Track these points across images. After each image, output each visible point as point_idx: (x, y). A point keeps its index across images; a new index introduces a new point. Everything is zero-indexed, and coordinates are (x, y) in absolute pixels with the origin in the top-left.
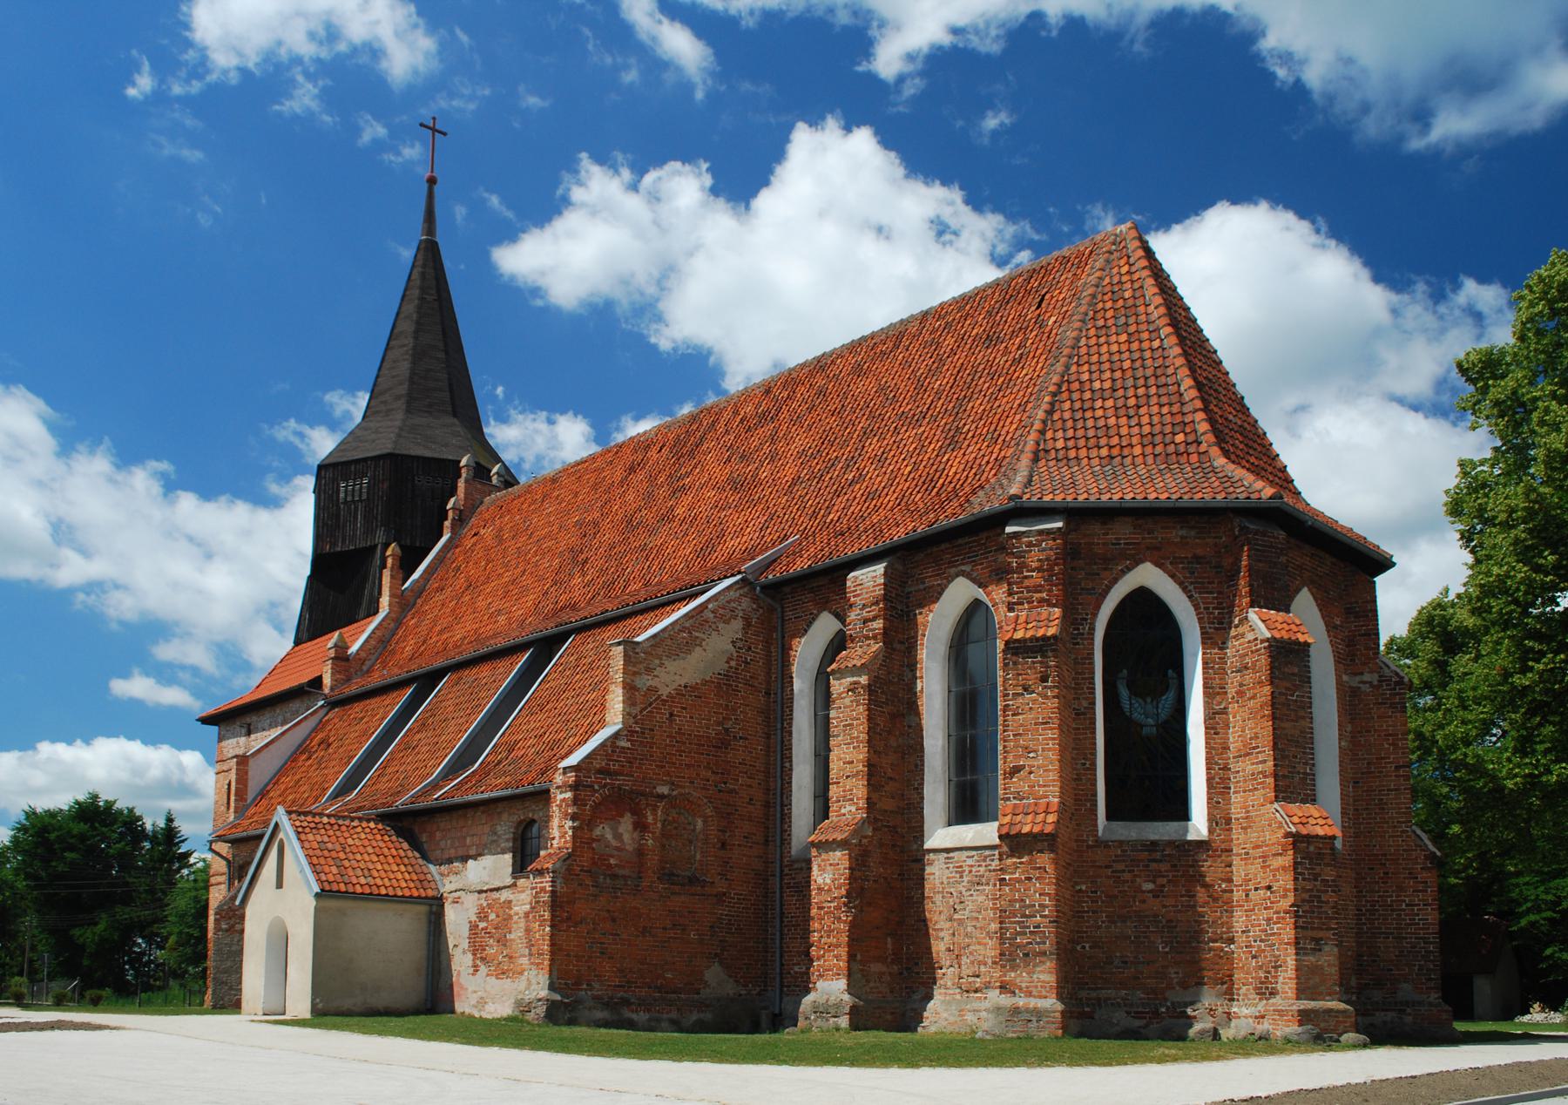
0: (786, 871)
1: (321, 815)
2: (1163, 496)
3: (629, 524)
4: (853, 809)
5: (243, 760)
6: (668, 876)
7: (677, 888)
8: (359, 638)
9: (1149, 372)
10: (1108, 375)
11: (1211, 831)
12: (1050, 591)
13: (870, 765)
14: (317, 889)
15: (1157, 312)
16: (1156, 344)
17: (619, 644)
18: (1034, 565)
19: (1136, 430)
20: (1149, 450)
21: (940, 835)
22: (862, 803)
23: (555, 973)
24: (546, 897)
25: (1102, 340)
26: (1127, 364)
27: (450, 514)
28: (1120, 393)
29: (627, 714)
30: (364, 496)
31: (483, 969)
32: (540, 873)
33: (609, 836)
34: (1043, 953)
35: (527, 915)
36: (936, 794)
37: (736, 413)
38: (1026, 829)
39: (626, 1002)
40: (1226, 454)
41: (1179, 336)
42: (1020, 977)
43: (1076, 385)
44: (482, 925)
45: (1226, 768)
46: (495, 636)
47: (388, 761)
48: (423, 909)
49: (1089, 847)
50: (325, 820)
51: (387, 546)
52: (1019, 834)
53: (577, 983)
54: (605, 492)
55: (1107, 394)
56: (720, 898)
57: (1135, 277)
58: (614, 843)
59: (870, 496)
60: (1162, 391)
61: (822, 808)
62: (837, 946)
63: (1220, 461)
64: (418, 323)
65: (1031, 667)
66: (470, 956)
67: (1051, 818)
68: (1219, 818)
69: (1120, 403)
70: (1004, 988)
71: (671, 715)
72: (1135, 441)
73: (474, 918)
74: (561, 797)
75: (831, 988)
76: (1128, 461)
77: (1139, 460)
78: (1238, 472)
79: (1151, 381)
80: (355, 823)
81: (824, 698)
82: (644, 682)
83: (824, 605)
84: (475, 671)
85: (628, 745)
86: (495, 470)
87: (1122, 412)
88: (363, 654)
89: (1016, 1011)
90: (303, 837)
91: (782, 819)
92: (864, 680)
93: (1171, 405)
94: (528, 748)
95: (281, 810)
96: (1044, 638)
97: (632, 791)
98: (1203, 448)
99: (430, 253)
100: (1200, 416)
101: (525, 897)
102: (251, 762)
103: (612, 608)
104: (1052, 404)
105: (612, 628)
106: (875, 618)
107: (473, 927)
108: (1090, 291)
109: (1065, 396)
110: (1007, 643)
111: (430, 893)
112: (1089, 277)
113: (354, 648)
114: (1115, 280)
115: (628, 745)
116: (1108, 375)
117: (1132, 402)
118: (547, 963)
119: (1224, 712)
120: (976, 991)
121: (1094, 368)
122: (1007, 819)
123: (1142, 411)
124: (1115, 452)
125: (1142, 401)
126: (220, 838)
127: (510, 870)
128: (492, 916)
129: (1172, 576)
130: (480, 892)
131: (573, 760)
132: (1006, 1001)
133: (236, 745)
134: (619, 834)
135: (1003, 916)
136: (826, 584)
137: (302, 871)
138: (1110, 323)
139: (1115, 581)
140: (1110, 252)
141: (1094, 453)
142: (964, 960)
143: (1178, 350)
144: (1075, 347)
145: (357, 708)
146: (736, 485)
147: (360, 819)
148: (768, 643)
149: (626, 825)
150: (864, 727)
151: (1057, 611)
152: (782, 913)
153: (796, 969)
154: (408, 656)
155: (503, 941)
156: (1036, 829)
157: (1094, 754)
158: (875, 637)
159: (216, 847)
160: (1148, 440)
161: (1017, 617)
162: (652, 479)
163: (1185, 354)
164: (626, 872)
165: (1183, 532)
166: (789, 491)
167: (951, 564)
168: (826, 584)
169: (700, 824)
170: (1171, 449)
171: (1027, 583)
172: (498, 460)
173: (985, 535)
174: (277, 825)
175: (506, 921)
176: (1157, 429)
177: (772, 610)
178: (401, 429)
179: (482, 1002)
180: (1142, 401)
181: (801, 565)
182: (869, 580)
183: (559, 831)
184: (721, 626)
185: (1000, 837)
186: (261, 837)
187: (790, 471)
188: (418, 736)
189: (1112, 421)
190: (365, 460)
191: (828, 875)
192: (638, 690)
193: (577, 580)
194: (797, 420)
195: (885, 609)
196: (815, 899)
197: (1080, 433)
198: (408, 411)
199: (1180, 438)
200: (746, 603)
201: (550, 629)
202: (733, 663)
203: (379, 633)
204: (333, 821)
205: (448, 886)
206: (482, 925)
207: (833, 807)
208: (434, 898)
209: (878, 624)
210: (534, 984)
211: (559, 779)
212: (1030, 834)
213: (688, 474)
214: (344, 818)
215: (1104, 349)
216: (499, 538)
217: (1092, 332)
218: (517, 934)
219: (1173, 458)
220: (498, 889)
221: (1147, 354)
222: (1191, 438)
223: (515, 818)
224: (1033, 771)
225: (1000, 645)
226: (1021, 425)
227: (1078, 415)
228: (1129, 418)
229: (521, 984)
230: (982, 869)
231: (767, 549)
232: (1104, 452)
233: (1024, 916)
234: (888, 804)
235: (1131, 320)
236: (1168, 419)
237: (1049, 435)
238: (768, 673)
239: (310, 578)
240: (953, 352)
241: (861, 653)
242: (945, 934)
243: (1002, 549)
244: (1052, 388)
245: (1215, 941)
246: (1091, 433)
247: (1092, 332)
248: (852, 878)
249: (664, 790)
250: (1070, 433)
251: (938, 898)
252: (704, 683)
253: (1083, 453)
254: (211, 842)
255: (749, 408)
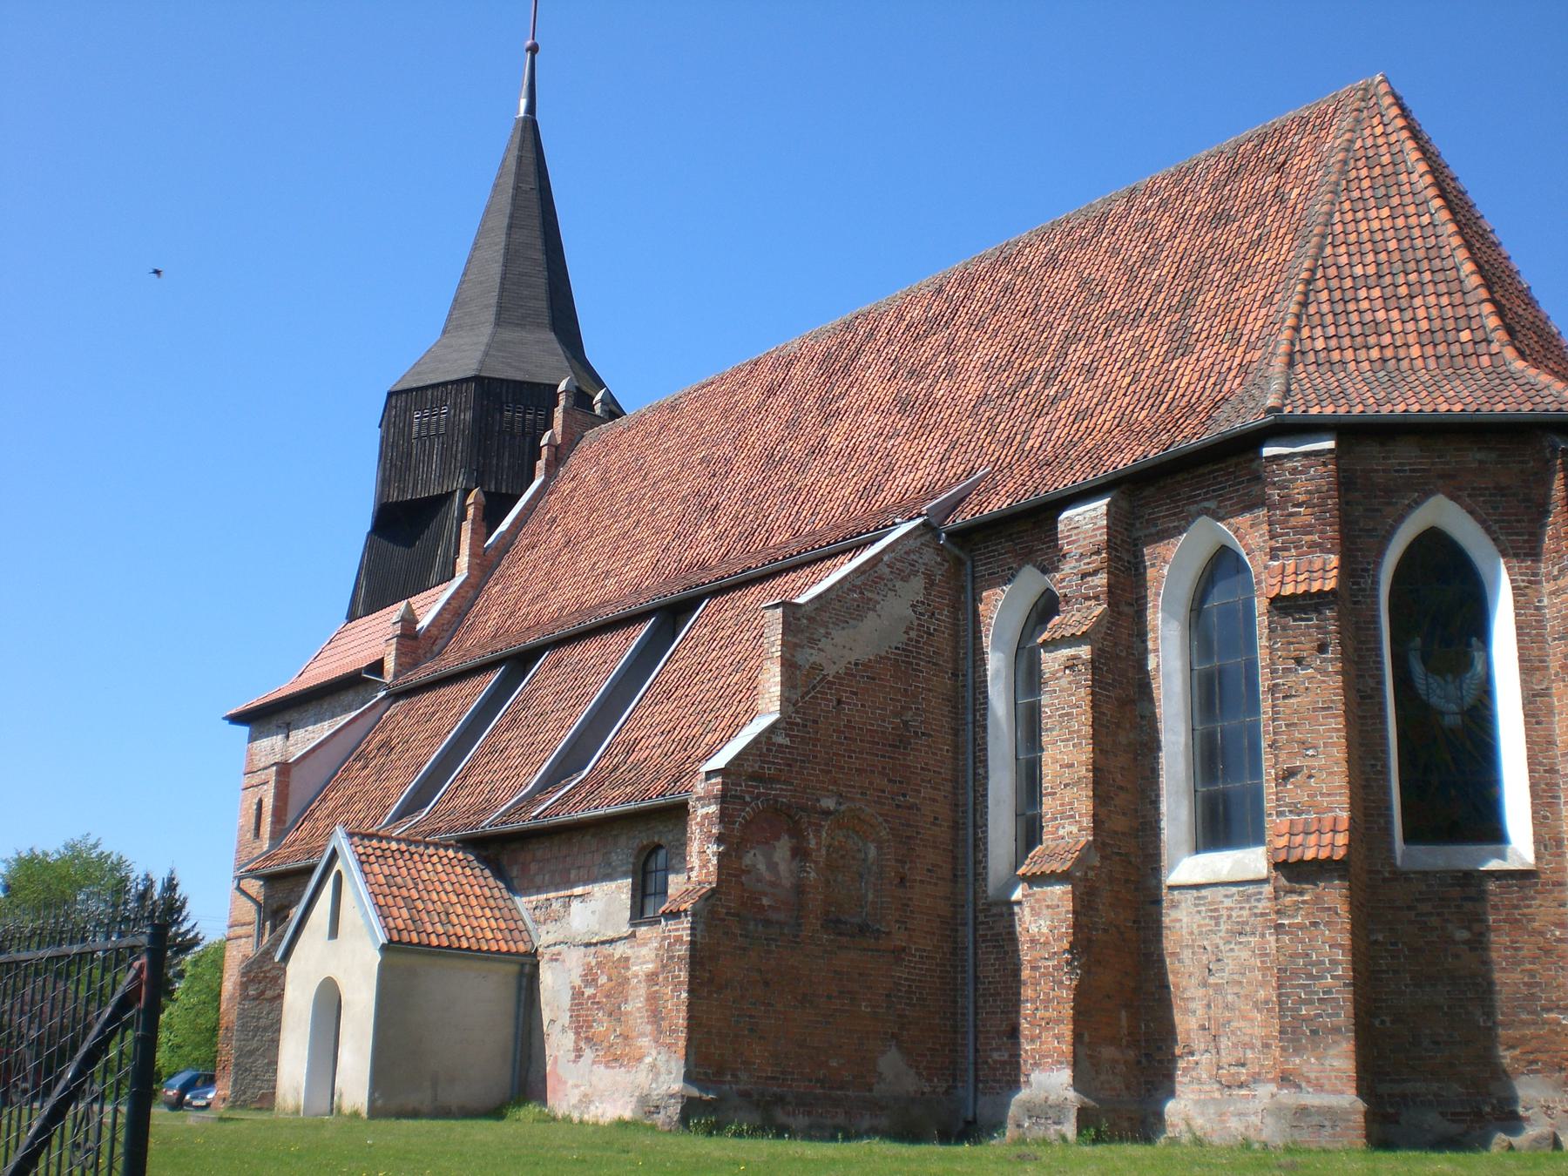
0: (981, 918)
1: (389, 839)
2: (1457, 408)
3: (771, 460)
4: (1075, 829)
5: (284, 769)
6: (833, 923)
7: (844, 940)
8: (429, 606)
9: (1421, 254)
10: (1370, 258)
11: (1538, 857)
12: (1322, 532)
13: (1097, 769)
14: (382, 939)
15: (1422, 180)
16: (1425, 219)
17: (776, 606)
18: (1301, 498)
19: (1410, 326)
20: (1429, 350)
21: (1187, 867)
22: (1087, 822)
23: (692, 1058)
24: (682, 951)
25: (1360, 215)
26: (1392, 245)
27: (545, 451)
28: (1387, 280)
29: (785, 700)
30: (442, 431)
31: (588, 1054)
32: (674, 915)
33: (762, 867)
34: (1336, 1030)
35: (652, 978)
36: (1176, 811)
37: (901, 318)
38: (1309, 855)
39: (780, 1100)
40: (1522, 355)
41: (1452, 212)
42: (1305, 1063)
43: (1332, 272)
44: (589, 992)
45: (1552, 770)
46: (603, 604)
47: (470, 768)
48: (513, 969)
49: (1384, 880)
50: (394, 845)
51: (467, 492)
52: (1301, 862)
53: (720, 1072)
54: (738, 420)
55: (1372, 281)
56: (899, 953)
57: (1393, 138)
58: (767, 876)
59: (1081, 415)
60: (1439, 277)
61: (1030, 832)
62: (1058, 1022)
63: (1519, 365)
64: (512, 217)
65: (1305, 630)
66: (571, 1035)
67: (1342, 839)
68: (1546, 839)
69: (1389, 292)
70: (1285, 1079)
71: (839, 702)
72: (1411, 339)
73: (578, 982)
74: (704, 813)
75: (1049, 1080)
76: (1405, 364)
77: (1419, 363)
78: (1544, 378)
79: (1425, 265)
80: (431, 850)
81: (1028, 677)
82: (807, 656)
83: (1026, 557)
84: (579, 649)
85: (787, 741)
86: (598, 397)
87: (1392, 303)
88: (435, 631)
89: (1303, 1111)
90: (367, 868)
91: (976, 846)
92: (1085, 652)
93: (1450, 294)
94: (651, 749)
95: (340, 832)
96: (1320, 593)
97: (789, 807)
98: (1495, 348)
99: (530, 127)
100: (1487, 308)
101: (654, 953)
102: (295, 772)
103: (756, 564)
104: (1306, 294)
105: (755, 589)
106: (1095, 573)
107: (577, 994)
108: (1340, 156)
109: (1320, 284)
110: (1272, 601)
111: (522, 947)
112: (1333, 141)
113: (424, 622)
114: (1369, 142)
115: (787, 741)
116: (1370, 258)
117: (1403, 291)
118: (682, 1043)
119: (1545, 693)
120: (1241, 1086)
121: (1353, 249)
122: (1282, 842)
123: (1418, 302)
124: (1389, 353)
125: (1416, 289)
126: (252, 874)
127: (628, 914)
128: (603, 980)
129: (1471, 512)
130: (588, 945)
131: (720, 761)
132: (1287, 1096)
133: (273, 747)
134: (774, 863)
135: (1283, 977)
136: (1029, 529)
137: (365, 914)
138: (1367, 194)
139: (1401, 518)
140: (1359, 110)
141: (1362, 354)
142: (1224, 1042)
143: (1451, 228)
144: (1328, 223)
145: (428, 698)
146: (904, 405)
147: (436, 845)
148: (956, 607)
149: (782, 850)
150: (1087, 718)
151: (1334, 560)
152: (976, 977)
153: (996, 1056)
154: (490, 628)
155: (615, 1014)
156: (1323, 854)
157: (1385, 751)
158: (1096, 598)
159: (245, 884)
160: (1428, 338)
161: (1284, 566)
162: (796, 403)
163: (1460, 232)
164: (782, 916)
165: (1479, 456)
166: (974, 412)
167: (1192, 499)
168: (1029, 529)
169: (873, 852)
170: (1456, 349)
171: (1293, 521)
172: (602, 385)
173: (1234, 461)
174: (334, 852)
175: (621, 985)
176: (1437, 324)
177: (959, 562)
178: (489, 345)
179: (586, 1100)
180: (1416, 289)
181: (998, 503)
182: (1086, 522)
183: (699, 863)
184: (899, 584)
185: (1277, 866)
186: (310, 870)
187: (974, 388)
188: (507, 735)
189: (1381, 315)
190: (445, 384)
191: (1042, 919)
192: (799, 667)
193: (706, 532)
194: (978, 325)
195: (1109, 560)
196: (1026, 954)
197: (1343, 330)
198: (499, 322)
199: (1465, 336)
200: (929, 557)
201: (676, 592)
202: (913, 634)
203: (455, 604)
204: (403, 847)
205: (544, 937)
206: (589, 992)
207: (1048, 827)
208: (526, 954)
209: (1101, 580)
210: (660, 1072)
211: (700, 788)
212: (1315, 860)
213: (842, 396)
214: (417, 843)
215: (1363, 226)
216: (605, 481)
217: (1347, 206)
218: (636, 1004)
219: (1456, 365)
220: (611, 941)
221: (1416, 232)
222: (1479, 335)
223: (636, 843)
224: (1311, 779)
225: (1261, 605)
226: (1269, 323)
227: (1339, 308)
228: (1401, 310)
229: (640, 1077)
230: (1245, 913)
231: (950, 486)
232: (1375, 354)
233: (1310, 976)
234: (1119, 823)
235: (1393, 191)
236: (1449, 312)
237: (1305, 332)
238: (955, 649)
239: (370, 534)
240: (1172, 236)
241: (1079, 616)
242: (1198, 1006)
243: (1257, 478)
244: (1304, 275)
245: (1549, 1010)
246: (1357, 330)
247: (1347, 206)
248: (1077, 926)
249: (829, 803)
250: (1331, 331)
251: (1186, 954)
252: (881, 659)
253: (1349, 354)
254: (240, 878)
255: (917, 313)
